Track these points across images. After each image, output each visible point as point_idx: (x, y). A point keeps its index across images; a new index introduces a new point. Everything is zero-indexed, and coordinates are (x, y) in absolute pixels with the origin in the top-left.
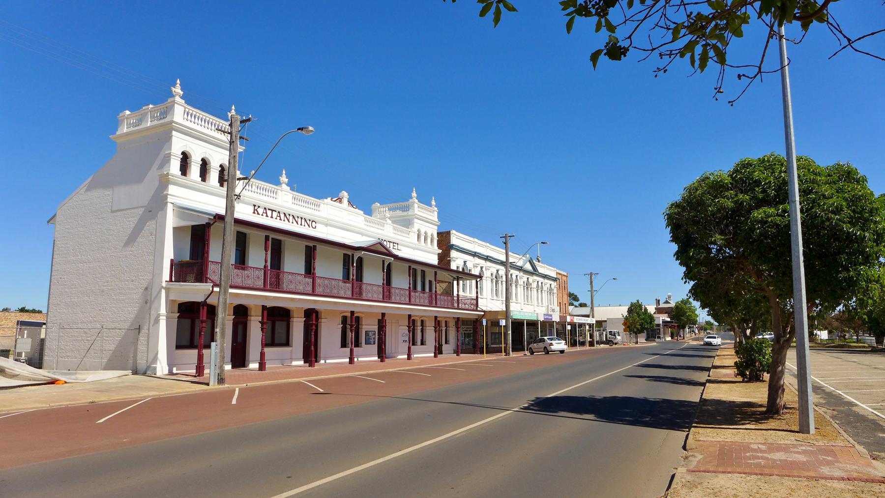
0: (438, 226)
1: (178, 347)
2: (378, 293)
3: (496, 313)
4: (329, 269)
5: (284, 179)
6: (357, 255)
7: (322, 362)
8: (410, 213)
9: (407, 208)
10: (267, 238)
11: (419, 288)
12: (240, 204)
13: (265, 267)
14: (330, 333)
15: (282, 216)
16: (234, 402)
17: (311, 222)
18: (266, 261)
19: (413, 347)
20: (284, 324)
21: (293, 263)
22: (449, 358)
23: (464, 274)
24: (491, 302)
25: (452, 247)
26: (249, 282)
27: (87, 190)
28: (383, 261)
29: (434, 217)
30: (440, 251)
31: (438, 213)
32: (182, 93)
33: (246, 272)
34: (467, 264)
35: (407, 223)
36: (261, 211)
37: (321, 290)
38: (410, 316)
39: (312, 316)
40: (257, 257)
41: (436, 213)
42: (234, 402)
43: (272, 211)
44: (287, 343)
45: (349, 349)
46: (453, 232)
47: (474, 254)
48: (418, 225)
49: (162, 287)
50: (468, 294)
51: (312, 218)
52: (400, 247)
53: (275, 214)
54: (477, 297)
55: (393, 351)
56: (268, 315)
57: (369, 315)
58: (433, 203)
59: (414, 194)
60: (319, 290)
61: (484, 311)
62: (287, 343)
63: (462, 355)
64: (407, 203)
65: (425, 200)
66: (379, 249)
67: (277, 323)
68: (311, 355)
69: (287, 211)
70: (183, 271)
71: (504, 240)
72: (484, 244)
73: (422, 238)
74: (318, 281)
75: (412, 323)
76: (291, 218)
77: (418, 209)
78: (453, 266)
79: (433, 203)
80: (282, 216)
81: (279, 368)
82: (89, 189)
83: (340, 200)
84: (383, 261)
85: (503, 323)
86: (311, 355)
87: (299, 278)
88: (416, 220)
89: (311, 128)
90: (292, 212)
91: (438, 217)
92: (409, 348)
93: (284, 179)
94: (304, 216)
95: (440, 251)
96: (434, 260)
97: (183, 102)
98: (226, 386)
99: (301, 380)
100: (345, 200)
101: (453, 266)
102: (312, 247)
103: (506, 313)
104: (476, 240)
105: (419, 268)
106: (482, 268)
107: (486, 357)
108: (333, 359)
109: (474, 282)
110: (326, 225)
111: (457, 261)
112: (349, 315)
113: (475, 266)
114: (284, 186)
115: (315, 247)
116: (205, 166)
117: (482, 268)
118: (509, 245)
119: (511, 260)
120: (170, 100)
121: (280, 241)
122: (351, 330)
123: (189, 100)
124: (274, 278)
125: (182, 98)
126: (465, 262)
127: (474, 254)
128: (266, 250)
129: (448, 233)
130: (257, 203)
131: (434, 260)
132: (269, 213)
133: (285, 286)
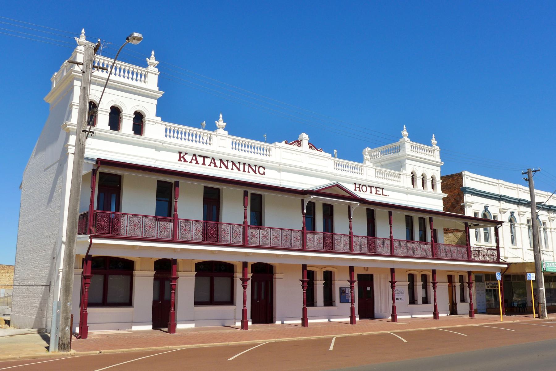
0: (441, 167)
1: (197, 303)
2: (361, 244)
3: (524, 265)
4: (283, 219)
5: (221, 123)
6: (320, 201)
7: (278, 323)
8: (401, 153)
9: (397, 149)
10: (246, 193)
11: (417, 237)
12: (94, 140)
13: (245, 222)
14: (287, 292)
15: (218, 163)
16: (331, 348)
17: (257, 168)
18: (245, 217)
19: (309, 309)
20: (227, 280)
21: (233, 213)
22: (462, 319)
23: (488, 221)
24: (516, 251)
25: (465, 190)
26: (137, 232)
27: (35, 155)
28: (349, 207)
29: (436, 157)
30: (445, 195)
31: (440, 152)
32: (407, 133)
33: (263, 232)
34: (489, 209)
35: (399, 166)
36: (188, 158)
37: (312, 245)
38: (304, 267)
39: (165, 269)
40: (189, 208)
41: (437, 153)
42: (331, 348)
43: (204, 157)
44: (231, 302)
45: (468, 304)
46: (466, 173)
47: (500, 198)
48: (410, 167)
49: (63, 242)
50: (483, 243)
51: (259, 163)
52: (385, 192)
53: (208, 161)
54: (498, 247)
55: (383, 311)
56: (93, 267)
57: (381, 270)
58: (434, 141)
59: (405, 133)
60: (396, 252)
61: (508, 264)
62: (231, 302)
63: (476, 316)
64: (396, 144)
65: (420, 138)
66: (336, 192)
67: (111, 278)
68: (163, 316)
69: (224, 158)
70: (86, 223)
71: (526, 176)
72: (515, 185)
73: (419, 182)
74: (180, 225)
75: (308, 278)
76: (230, 165)
77: (409, 147)
78: (469, 212)
79: (434, 141)
80: (218, 163)
81: (218, 329)
82: (36, 154)
83: (299, 144)
84: (349, 207)
85: (532, 277)
86: (163, 316)
87: (402, 244)
88: (407, 161)
89: (136, 34)
90: (230, 158)
91: (441, 157)
92: (304, 311)
93: (221, 123)
94: (247, 161)
95: (445, 195)
96: (438, 206)
97: (409, 139)
98: (72, 351)
99: (390, 332)
100: (305, 143)
101: (469, 212)
102: (257, 197)
103: (536, 266)
104: (501, 181)
105: (427, 217)
106: (512, 213)
107: (502, 319)
108: (287, 320)
109: (492, 229)
110: (279, 170)
111: (473, 206)
112: (466, 275)
113: (502, 211)
114: (221, 131)
115: (177, 183)
116: (115, 115)
117: (512, 213)
118: (533, 182)
119: (538, 199)
120: (401, 140)
121: (261, 196)
122: (316, 288)
123: (413, 138)
124: (211, 232)
125: (408, 137)
126: (486, 207)
127: (500, 198)
128: (245, 206)
129: (460, 175)
130: (184, 150)
131: (438, 206)
132: (200, 160)
133: (123, 231)
